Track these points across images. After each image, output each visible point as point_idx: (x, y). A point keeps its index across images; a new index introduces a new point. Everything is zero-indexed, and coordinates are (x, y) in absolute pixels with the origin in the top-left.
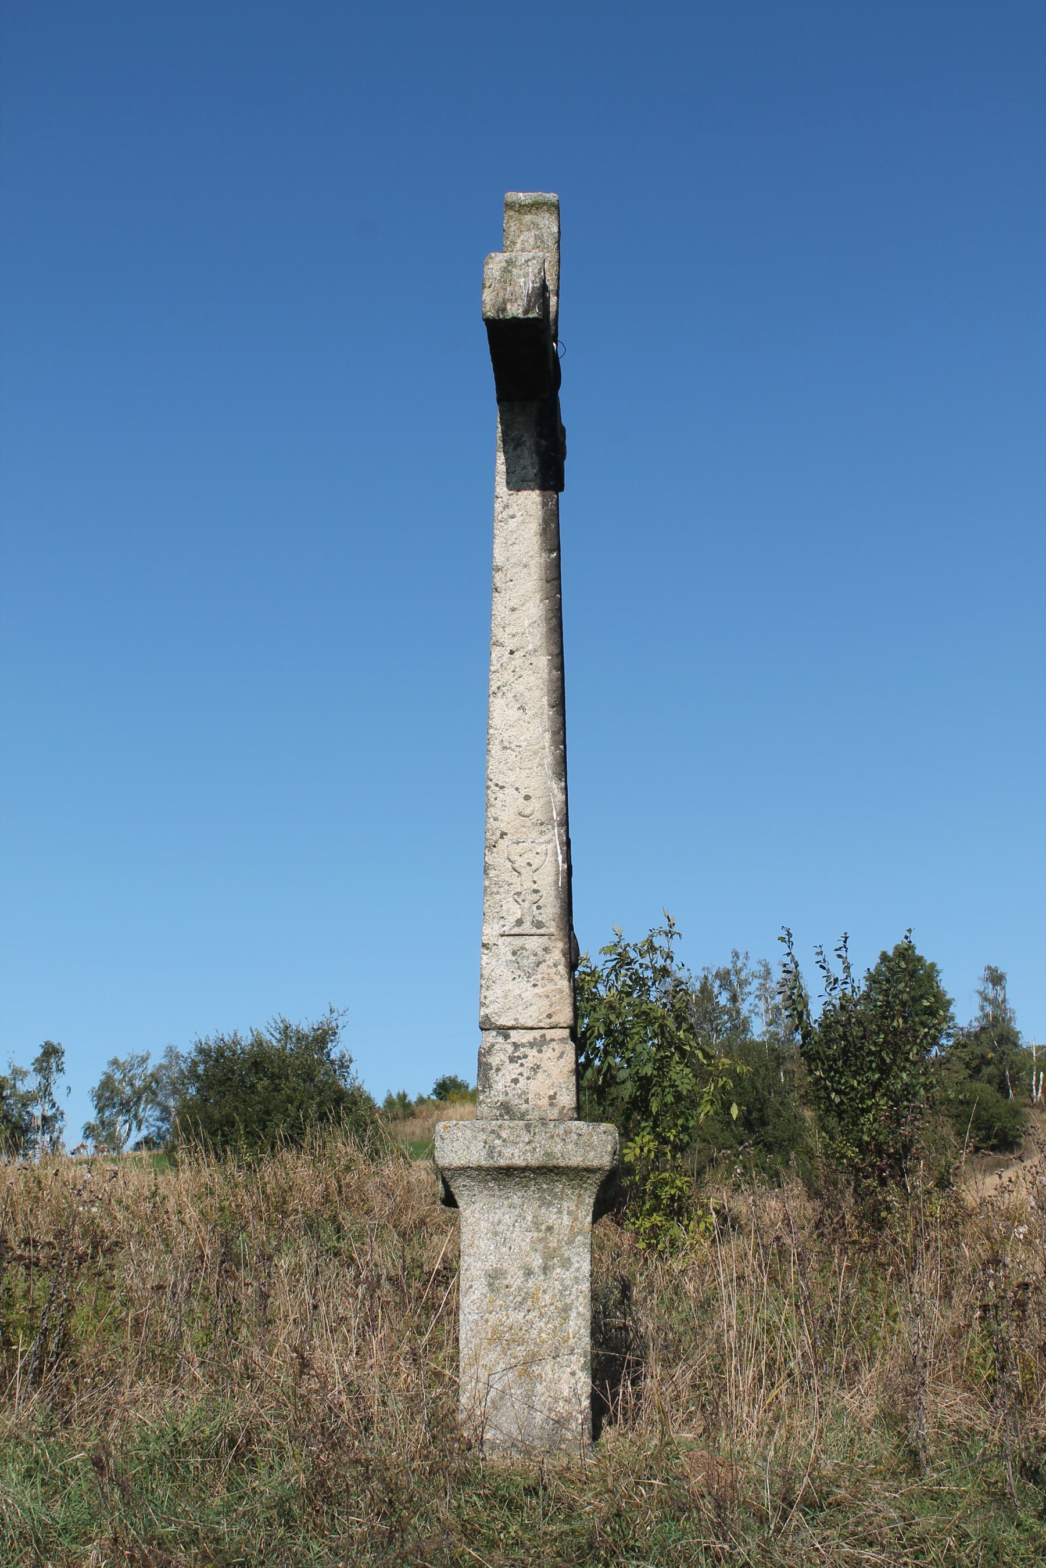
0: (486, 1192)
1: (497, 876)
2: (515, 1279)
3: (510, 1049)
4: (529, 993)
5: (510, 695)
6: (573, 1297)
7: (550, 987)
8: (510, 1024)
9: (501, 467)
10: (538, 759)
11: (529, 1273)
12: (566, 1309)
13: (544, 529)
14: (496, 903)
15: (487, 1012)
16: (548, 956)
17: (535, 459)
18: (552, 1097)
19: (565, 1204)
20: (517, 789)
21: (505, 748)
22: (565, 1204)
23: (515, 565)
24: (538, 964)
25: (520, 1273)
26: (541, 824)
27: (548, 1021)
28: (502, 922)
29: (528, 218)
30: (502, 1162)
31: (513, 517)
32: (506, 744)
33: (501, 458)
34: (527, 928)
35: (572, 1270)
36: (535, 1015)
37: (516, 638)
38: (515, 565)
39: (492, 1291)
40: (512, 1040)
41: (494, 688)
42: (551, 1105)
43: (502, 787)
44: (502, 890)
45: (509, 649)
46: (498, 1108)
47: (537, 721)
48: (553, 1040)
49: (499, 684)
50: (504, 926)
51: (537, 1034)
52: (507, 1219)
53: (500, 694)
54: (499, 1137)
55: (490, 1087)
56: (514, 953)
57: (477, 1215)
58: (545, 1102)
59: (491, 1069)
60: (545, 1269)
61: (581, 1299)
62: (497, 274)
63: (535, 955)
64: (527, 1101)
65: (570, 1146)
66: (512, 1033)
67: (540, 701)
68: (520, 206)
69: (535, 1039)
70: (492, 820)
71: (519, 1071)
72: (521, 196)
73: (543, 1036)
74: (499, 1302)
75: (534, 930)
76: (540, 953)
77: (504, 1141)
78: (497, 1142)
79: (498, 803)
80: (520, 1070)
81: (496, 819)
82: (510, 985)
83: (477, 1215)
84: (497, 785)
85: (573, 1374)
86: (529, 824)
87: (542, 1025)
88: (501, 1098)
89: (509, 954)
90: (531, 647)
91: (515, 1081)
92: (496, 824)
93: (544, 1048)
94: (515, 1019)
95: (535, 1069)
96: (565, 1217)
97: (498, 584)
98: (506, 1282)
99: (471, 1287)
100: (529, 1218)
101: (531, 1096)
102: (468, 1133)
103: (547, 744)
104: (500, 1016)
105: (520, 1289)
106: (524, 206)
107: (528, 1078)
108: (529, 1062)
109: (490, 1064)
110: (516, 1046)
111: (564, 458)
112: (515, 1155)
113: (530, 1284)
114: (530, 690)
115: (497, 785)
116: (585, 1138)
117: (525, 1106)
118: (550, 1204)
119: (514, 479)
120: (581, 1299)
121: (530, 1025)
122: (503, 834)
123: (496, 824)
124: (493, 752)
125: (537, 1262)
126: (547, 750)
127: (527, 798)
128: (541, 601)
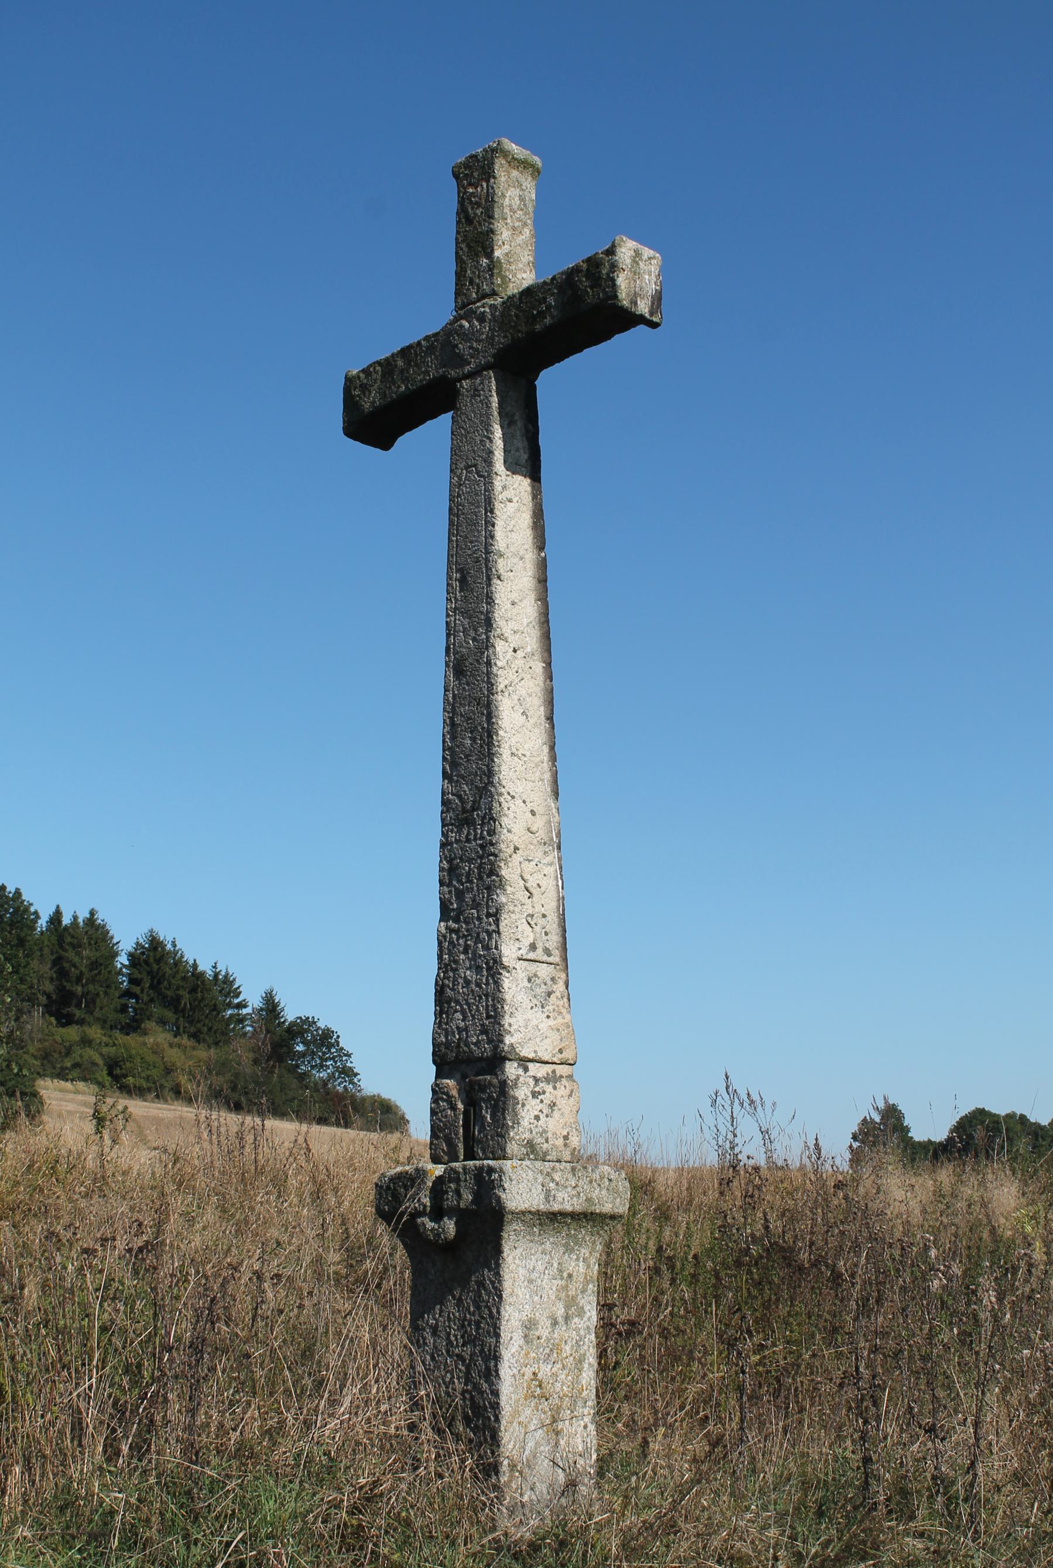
0: (528, 1237)
1: (513, 894)
2: (543, 1330)
3: (532, 1082)
4: (545, 1025)
5: (516, 698)
6: (586, 1348)
7: (560, 1020)
8: (531, 1056)
9: (498, 444)
10: (538, 773)
11: (555, 1323)
12: (580, 1361)
13: (534, 523)
14: (512, 923)
15: (512, 1041)
16: (555, 987)
17: (526, 443)
18: (566, 1138)
19: (583, 1251)
20: (524, 802)
21: (513, 754)
22: (583, 1251)
23: (514, 555)
24: (549, 994)
25: (548, 1323)
26: (545, 844)
27: (560, 1056)
28: (517, 945)
29: (515, 173)
30: (556, 1207)
31: (510, 501)
32: (514, 750)
33: (498, 433)
34: (539, 954)
35: (585, 1319)
36: (550, 1048)
37: (518, 636)
38: (514, 555)
39: (527, 1342)
40: (531, 1073)
41: (501, 687)
42: (565, 1145)
43: (513, 797)
44: (516, 909)
45: (512, 645)
46: (525, 1146)
47: (537, 731)
48: (561, 1077)
49: (507, 682)
50: (520, 949)
51: (549, 1068)
52: (540, 1267)
53: (506, 694)
54: (553, 1180)
55: (518, 1123)
56: (529, 980)
57: (517, 1261)
58: (560, 1142)
59: (518, 1103)
60: (567, 1318)
61: (591, 1349)
62: (628, 261)
63: (545, 984)
64: (547, 1141)
65: (604, 1192)
66: (530, 1065)
67: (538, 711)
68: (513, 158)
69: (548, 1074)
70: (505, 831)
71: (539, 1108)
72: (514, 148)
73: (554, 1072)
74: (533, 1355)
75: (545, 958)
76: (549, 982)
77: (557, 1184)
78: (551, 1185)
79: (511, 814)
80: (541, 1105)
81: (509, 831)
82: (530, 1014)
83: (517, 1261)
84: (509, 793)
85: (585, 1427)
86: (535, 841)
87: (555, 1060)
88: (527, 1135)
89: (525, 980)
90: (529, 649)
91: (537, 1118)
92: (510, 836)
93: (558, 1085)
94: (535, 1052)
95: (553, 1105)
96: (581, 1264)
97: (501, 571)
98: (537, 1333)
99: (511, 1338)
100: (555, 1265)
101: (550, 1135)
102: (530, 1173)
103: (546, 759)
104: (522, 1047)
105: (548, 1340)
106: (516, 159)
107: (547, 1116)
108: (547, 1098)
109: (517, 1098)
110: (537, 1080)
111: (432, 419)
112: (566, 1201)
113: (556, 1335)
114: (530, 696)
115: (509, 793)
116: (613, 1184)
117: (545, 1146)
118: (572, 1251)
119: (510, 460)
120: (591, 1349)
121: (546, 1058)
122: (516, 849)
123: (510, 836)
124: (504, 756)
125: (560, 1312)
126: (545, 764)
127: (533, 813)
128: (536, 601)
